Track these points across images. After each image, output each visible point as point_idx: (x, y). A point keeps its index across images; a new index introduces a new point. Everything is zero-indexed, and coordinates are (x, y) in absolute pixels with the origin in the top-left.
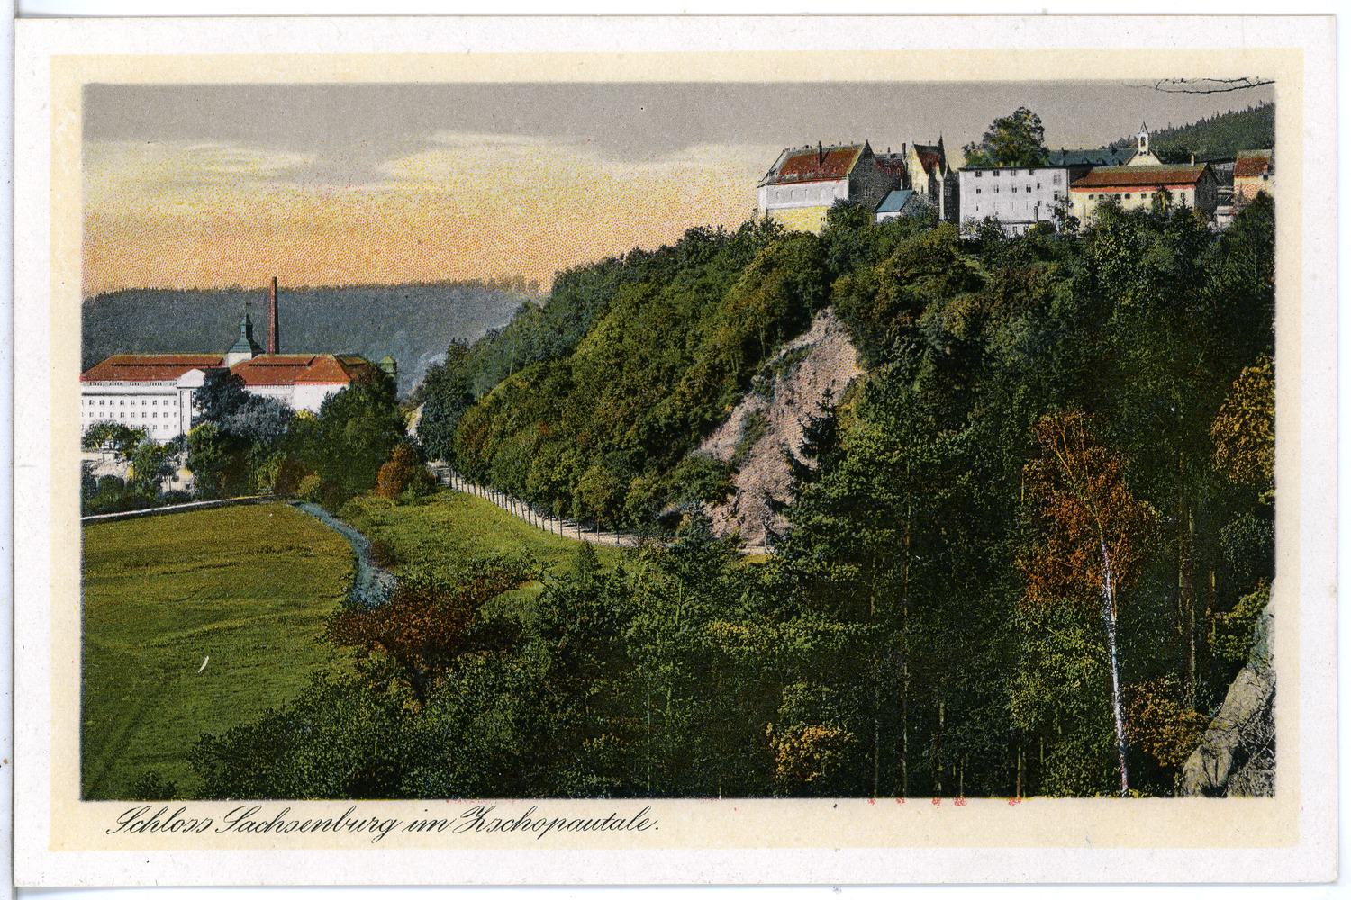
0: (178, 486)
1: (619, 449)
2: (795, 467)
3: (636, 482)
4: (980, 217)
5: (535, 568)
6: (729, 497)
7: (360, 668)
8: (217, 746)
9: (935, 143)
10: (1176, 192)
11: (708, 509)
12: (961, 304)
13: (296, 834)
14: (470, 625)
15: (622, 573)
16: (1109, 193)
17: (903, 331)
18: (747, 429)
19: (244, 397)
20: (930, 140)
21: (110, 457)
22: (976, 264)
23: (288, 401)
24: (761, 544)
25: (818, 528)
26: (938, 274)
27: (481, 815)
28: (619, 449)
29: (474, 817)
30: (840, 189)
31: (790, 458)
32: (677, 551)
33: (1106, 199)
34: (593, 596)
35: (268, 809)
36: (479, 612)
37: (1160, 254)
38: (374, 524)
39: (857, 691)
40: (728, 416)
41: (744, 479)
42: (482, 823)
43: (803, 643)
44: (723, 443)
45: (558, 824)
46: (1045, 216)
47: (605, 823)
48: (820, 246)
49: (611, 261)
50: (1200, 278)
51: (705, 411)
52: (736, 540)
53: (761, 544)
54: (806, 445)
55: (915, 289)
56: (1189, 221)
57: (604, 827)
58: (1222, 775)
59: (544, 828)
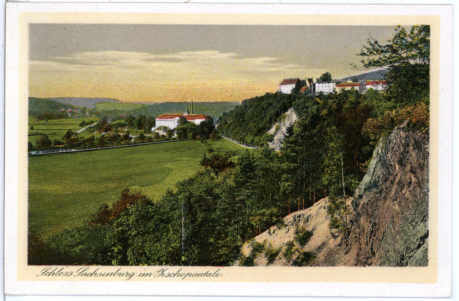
0: (174, 137)
1: (253, 132)
2: (285, 136)
3: (256, 138)
4: (319, 91)
5: (238, 153)
6: (273, 141)
7: (206, 170)
8: (181, 183)
9: (311, 78)
10: (355, 87)
11: (269, 143)
12: (315, 107)
14: (226, 163)
15: (253, 154)
16: (343, 87)
17: (305, 112)
18: (276, 129)
19: (187, 121)
20: (310, 77)
21: (162, 131)
22: (318, 100)
23: (194, 122)
24: (278, 150)
25: (288, 147)
26: (311, 102)
27: (163, 271)
28: (253, 132)
29: (161, 272)
30: (294, 86)
31: (284, 134)
32: (263, 150)
33: (342, 88)
34: (248, 158)
35: (92, 268)
36: (227, 161)
37: (352, 98)
38: (209, 144)
39: (296, 177)
40: (273, 126)
41: (276, 138)
42: (164, 274)
43: (285, 167)
44: (272, 131)
45: (189, 275)
46: (331, 91)
47: (205, 274)
48: (289, 96)
49: (252, 98)
50: (359, 103)
51: (269, 125)
52: (274, 149)
53: (278, 150)
54: (287, 132)
55: (307, 104)
56: (357, 93)
57: (205, 276)
58: (362, 193)
59: (184, 276)
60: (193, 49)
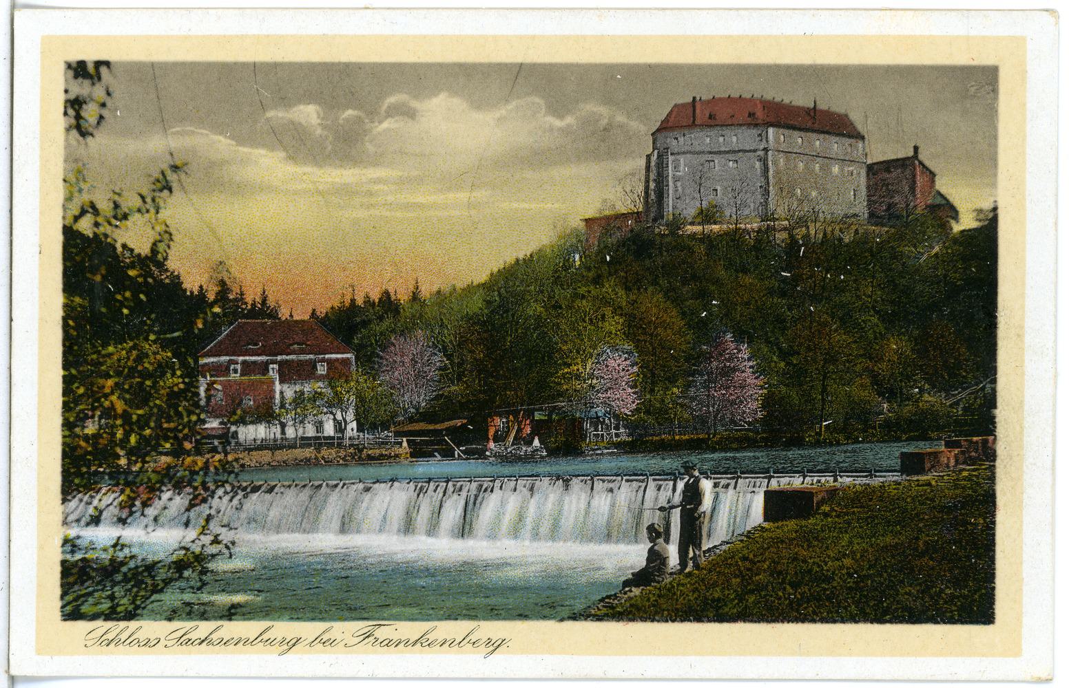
60: (251, 146)
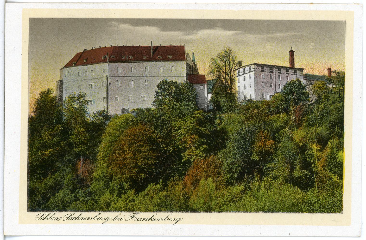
13: (83, 221)
35: (46, 214)
